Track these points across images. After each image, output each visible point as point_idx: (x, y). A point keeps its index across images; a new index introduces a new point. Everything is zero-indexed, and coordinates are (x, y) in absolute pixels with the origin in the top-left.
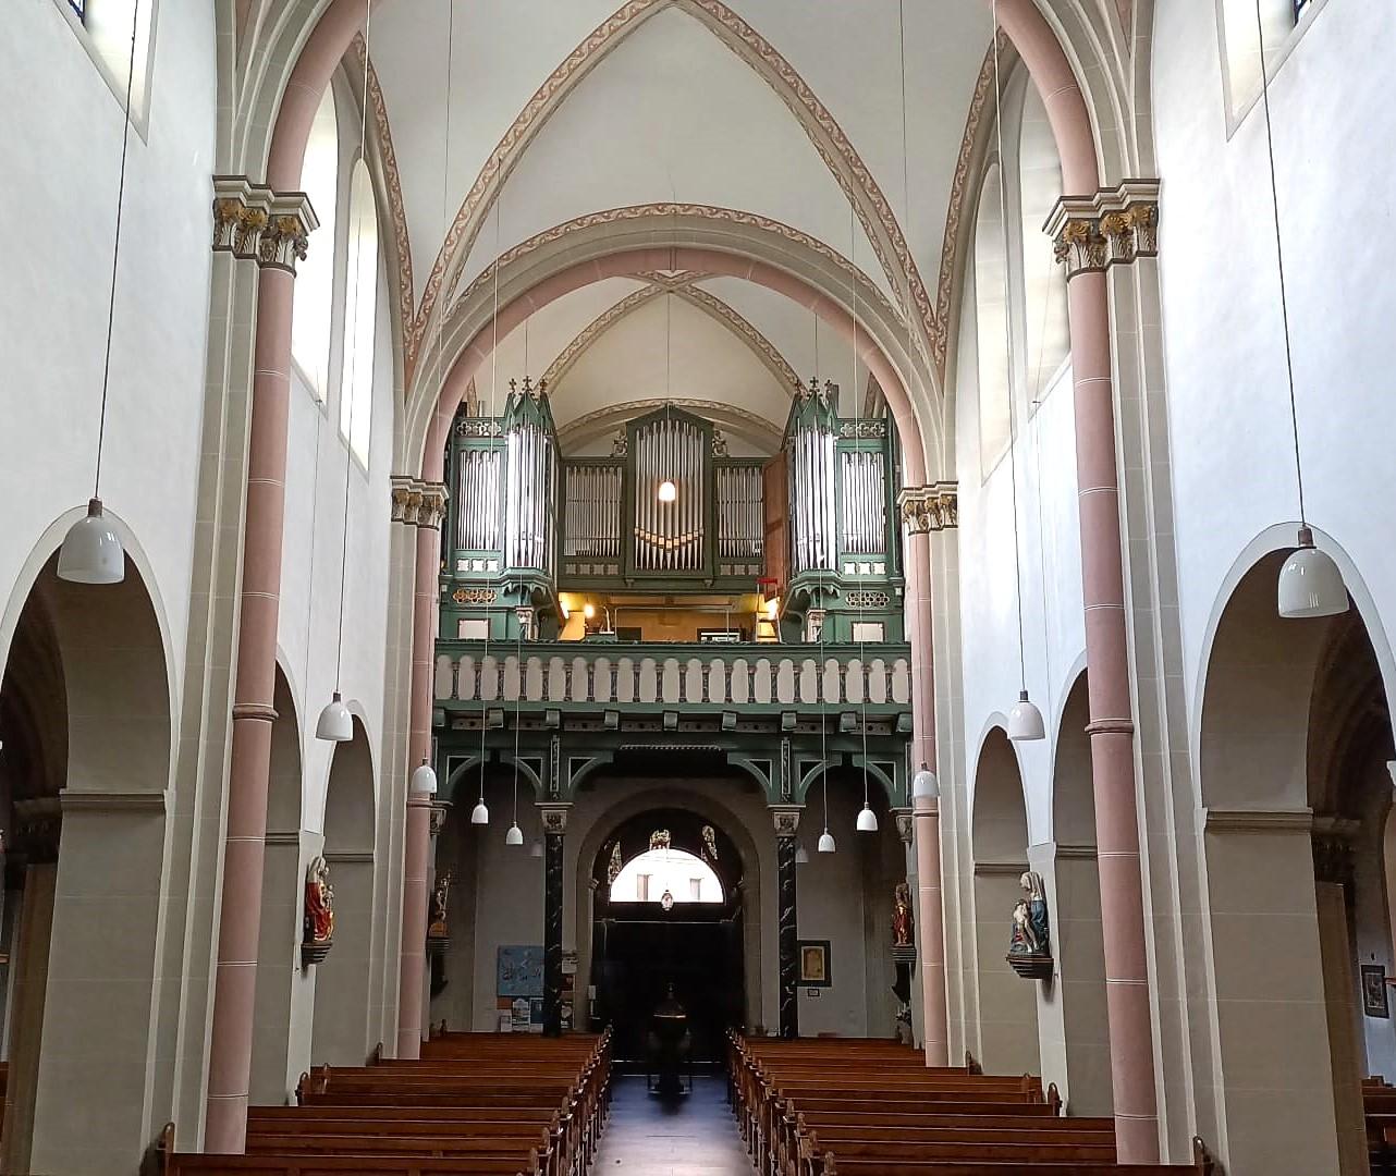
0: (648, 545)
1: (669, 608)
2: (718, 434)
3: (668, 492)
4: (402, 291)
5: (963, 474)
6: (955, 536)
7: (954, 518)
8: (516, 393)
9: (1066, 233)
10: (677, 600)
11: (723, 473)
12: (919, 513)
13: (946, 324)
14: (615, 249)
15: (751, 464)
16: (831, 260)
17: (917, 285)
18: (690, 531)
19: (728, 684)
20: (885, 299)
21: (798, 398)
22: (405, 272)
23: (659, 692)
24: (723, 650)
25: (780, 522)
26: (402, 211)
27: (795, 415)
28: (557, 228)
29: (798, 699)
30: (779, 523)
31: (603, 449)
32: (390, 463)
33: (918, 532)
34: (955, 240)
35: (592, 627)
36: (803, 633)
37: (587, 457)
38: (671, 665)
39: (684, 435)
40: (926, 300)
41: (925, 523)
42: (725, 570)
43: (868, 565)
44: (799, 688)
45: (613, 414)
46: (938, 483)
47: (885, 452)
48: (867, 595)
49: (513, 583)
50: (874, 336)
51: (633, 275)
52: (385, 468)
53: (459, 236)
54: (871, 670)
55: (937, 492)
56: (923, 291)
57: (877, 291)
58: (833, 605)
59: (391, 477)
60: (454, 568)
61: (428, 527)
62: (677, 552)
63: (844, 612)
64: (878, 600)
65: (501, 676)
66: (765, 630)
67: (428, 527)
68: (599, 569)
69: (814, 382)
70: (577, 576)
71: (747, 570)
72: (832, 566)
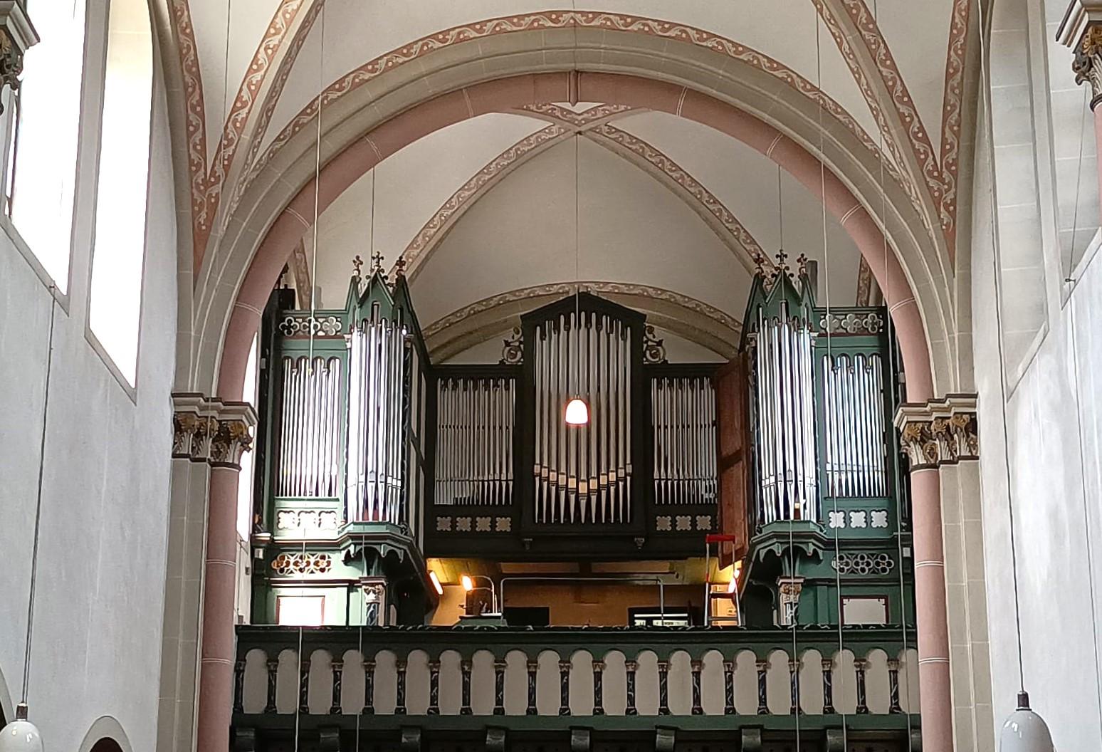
0: (545, 484)
1: (585, 581)
2: (651, 330)
3: (576, 413)
4: (190, 135)
5: (985, 385)
6: (975, 476)
7: (973, 446)
8: (363, 276)
9: (1087, 42)
10: (597, 567)
11: (660, 386)
12: (923, 438)
13: (955, 174)
14: (492, 74)
15: (698, 370)
16: (792, 86)
17: (912, 119)
18: (594, 474)
19: (664, 688)
20: (869, 140)
21: (759, 279)
22: (193, 108)
23: (565, 700)
24: (664, 641)
25: (739, 455)
26: (189, 25)
27: (755, 304)
28: (409, 46)
29: (764, 711)
30: (736, 457)
31: (490, 354)
32: (172, 377)
33: (922, 466)
34: (962, 58)
35: (475, 603)
36: (775, 611)
37: (457, 363)
38: (582, 659)
39: (603, 333)
40: (925, 139)
41: (933, 453)
42: (664, 524)
43: (863, 514)
44: (764, 693)
45: (504, 303)
46: (949, 396)
47: (883, 355)
48: (862, 558)
49: (355, 545)
50: (856, 192)
51: (527, 111)
52: (166, 382)
53: (271, 59)
54: (868, 666)
55: (948, 410)
56: (921, 129)
57: (857, 129)
58: (814, 572)
59: (173, 395)
60: (272, 526)
61: (227, 465)
62: (594, 498)
63: (830, 583)
64: (878, 564)
65: (337, 678)
66: (725, 611)
67: (227, 465)
68: (483, 524)
69: (782, 256)
70: (454, 534)
71: (694, 523)
72: (810, 514)
